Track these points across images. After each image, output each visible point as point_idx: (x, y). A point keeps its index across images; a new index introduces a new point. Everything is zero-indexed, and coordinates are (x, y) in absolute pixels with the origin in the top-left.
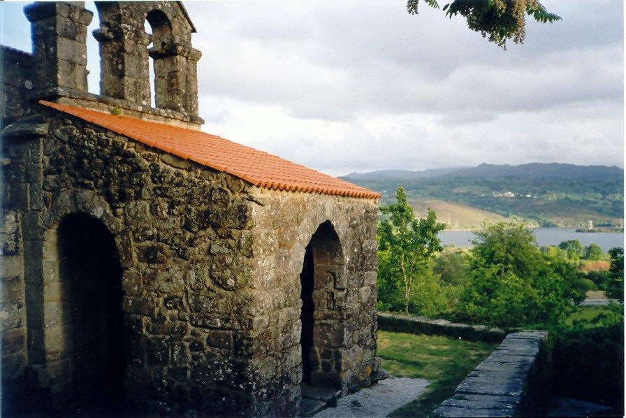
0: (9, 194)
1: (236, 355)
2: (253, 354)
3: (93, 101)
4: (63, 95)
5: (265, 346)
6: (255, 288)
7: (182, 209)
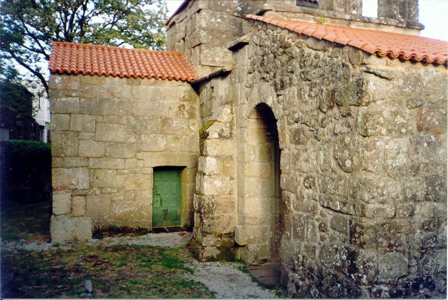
0: (231, 93)
1: (351, 242)
2: (364, 243)
3: (298, 13)
4: (268, 8)
6: (370, 171)
7: (317, 91)
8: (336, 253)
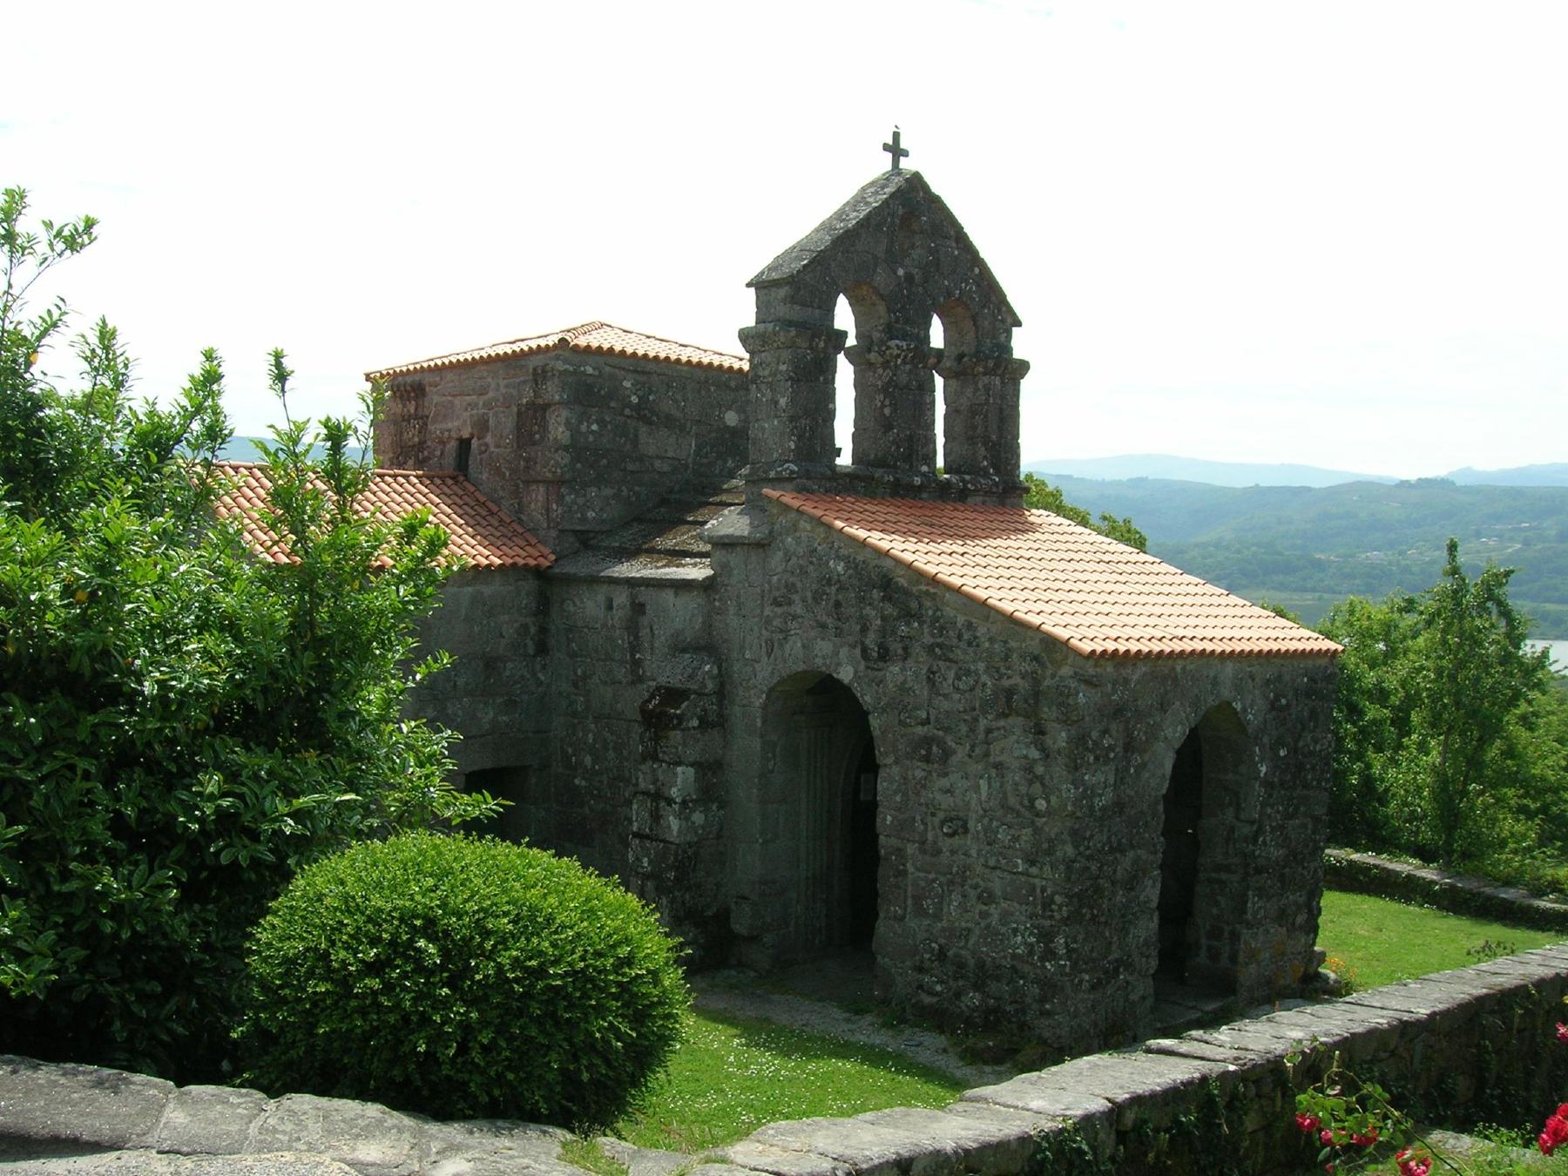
5: (1092, 908)
8: (1015, 936)
